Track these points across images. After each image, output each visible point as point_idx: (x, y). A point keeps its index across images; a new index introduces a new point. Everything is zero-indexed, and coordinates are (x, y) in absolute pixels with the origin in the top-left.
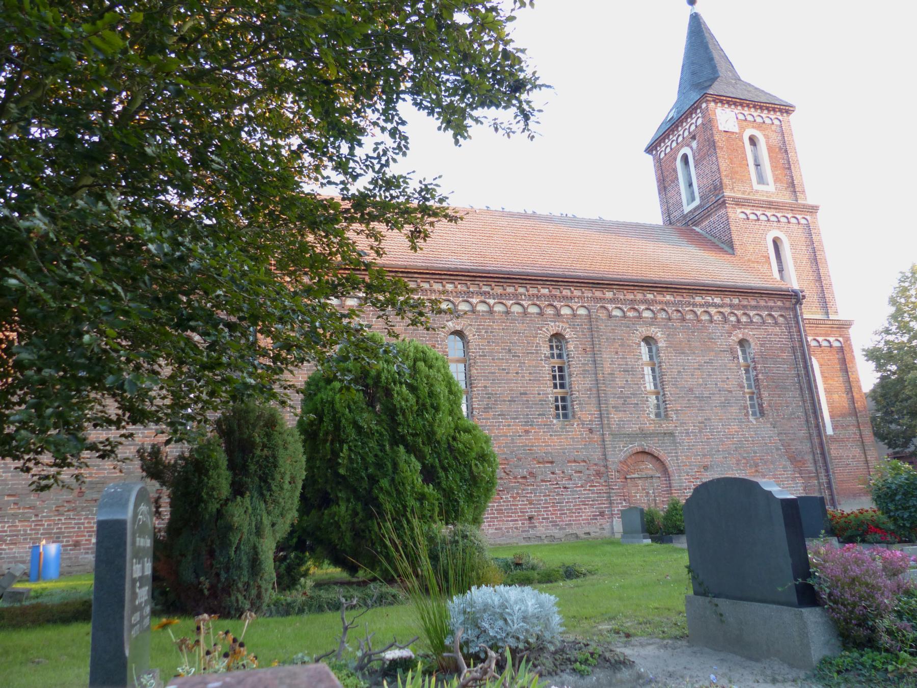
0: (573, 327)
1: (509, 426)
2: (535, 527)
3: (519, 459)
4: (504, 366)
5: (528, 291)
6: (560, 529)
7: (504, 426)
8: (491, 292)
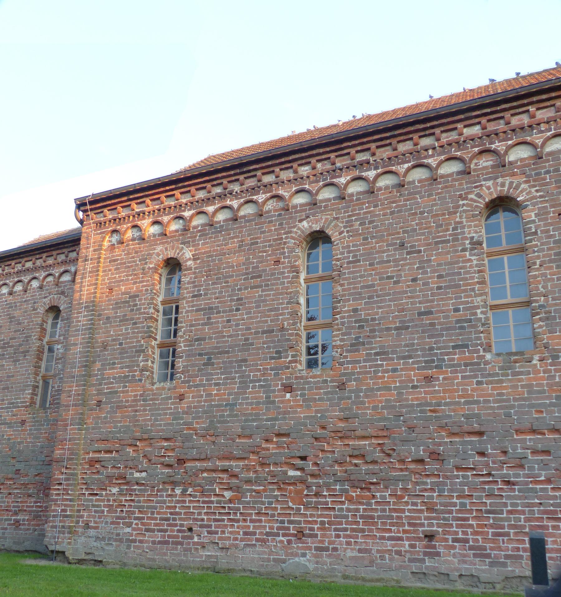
0: (535, 179)
1: (395, 370)
2: (438, 554)
3: (411, 429)
4: (390, 271)
5: (438, 140)
6: (492, 564)
7: (387, 371)
8: (371, 159)
